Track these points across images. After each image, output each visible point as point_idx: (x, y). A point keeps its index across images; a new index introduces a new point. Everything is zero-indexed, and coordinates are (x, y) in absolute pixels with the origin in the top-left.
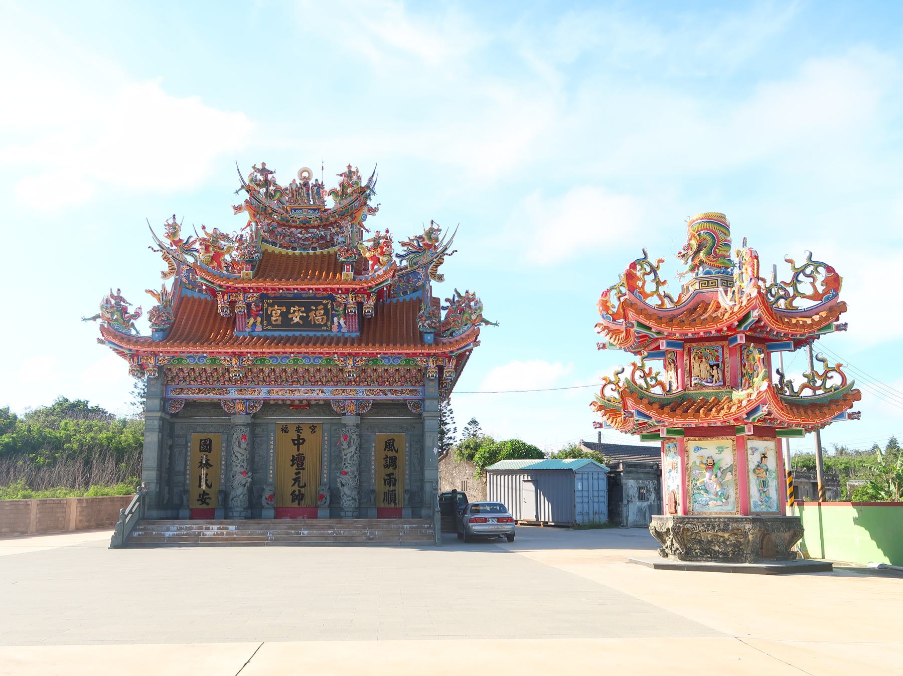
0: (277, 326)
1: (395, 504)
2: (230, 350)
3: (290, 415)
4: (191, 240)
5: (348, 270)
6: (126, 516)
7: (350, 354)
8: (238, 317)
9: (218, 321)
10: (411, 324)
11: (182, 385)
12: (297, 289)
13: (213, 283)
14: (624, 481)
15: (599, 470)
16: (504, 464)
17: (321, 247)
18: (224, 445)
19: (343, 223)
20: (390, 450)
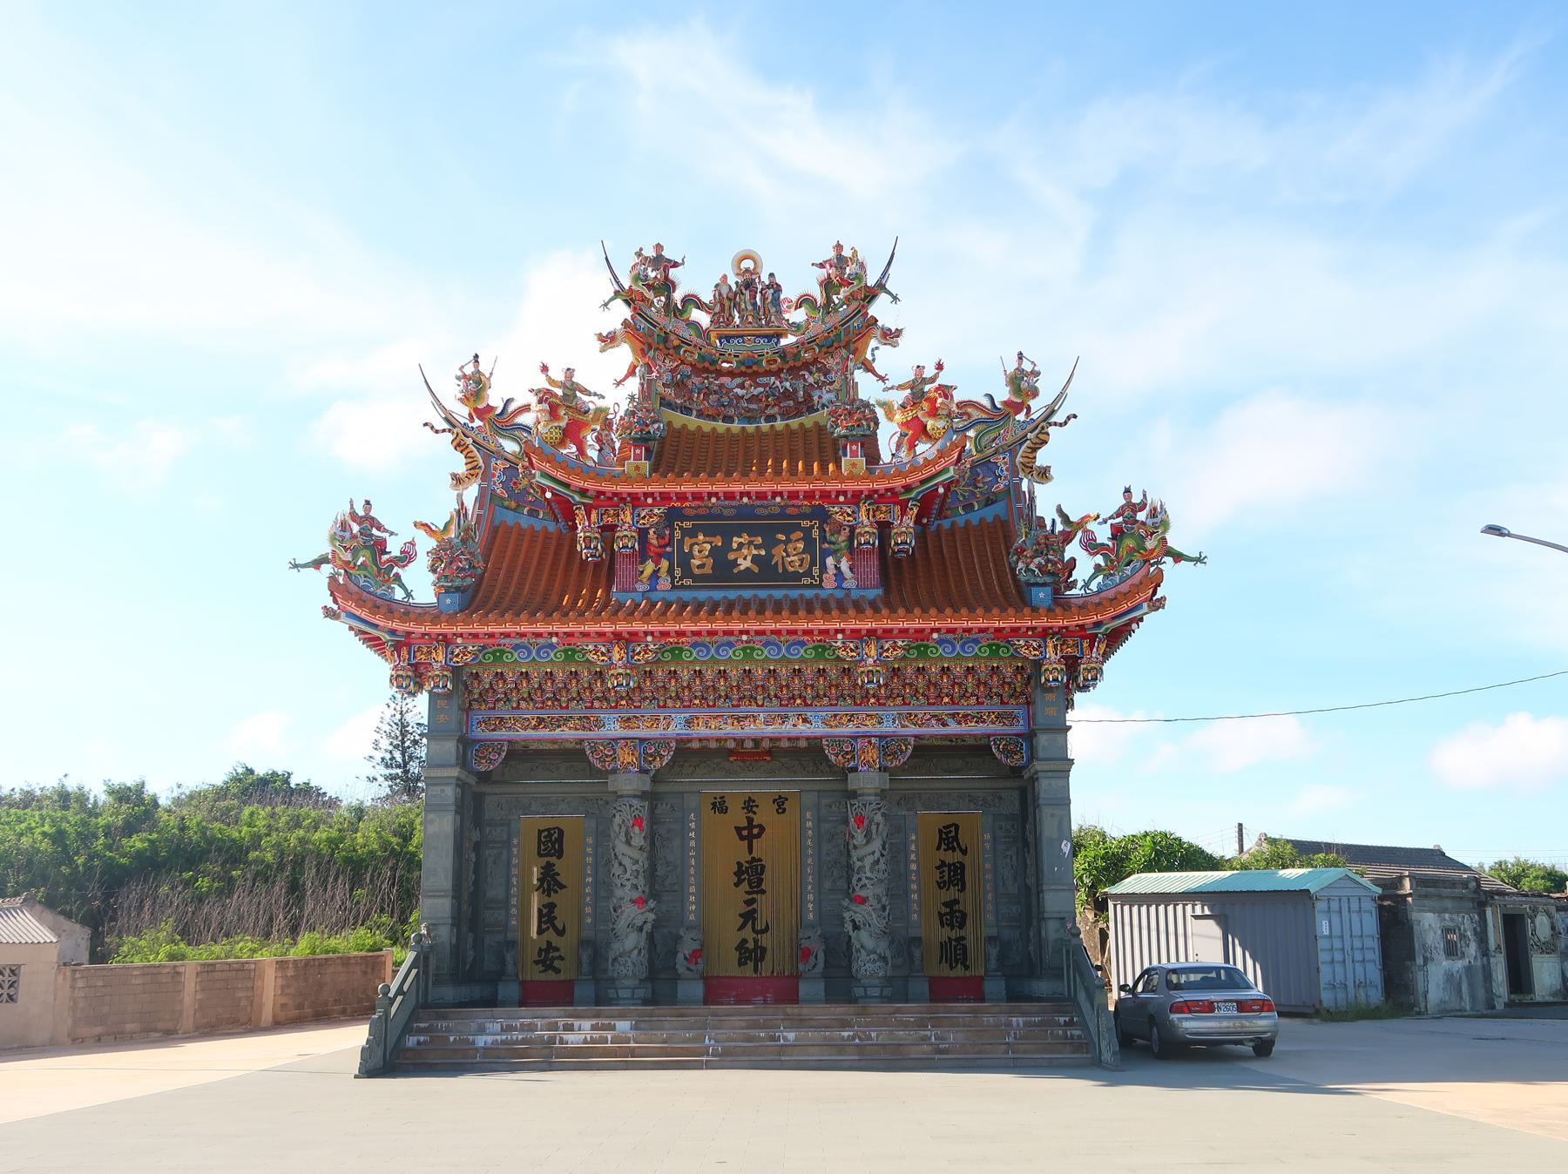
0: (703, 578)
1: (967, 967)
2: (607, 628)
3: (729, 773)
4: (512, 407)
5: (854, 454)
6: (392, 1001)
7: (871, 632)
8: (619, 560)
9: (574, 573)
10: (992, 577)
11: (503, 710)
12: (748, 494)
13: (567, 486)
14: (1415, 916)
15: (1362, 892)
16: (1138, 883)
17: (786, 415)
18: (590, 840)
19: (831, 362)
20: (950, 848)
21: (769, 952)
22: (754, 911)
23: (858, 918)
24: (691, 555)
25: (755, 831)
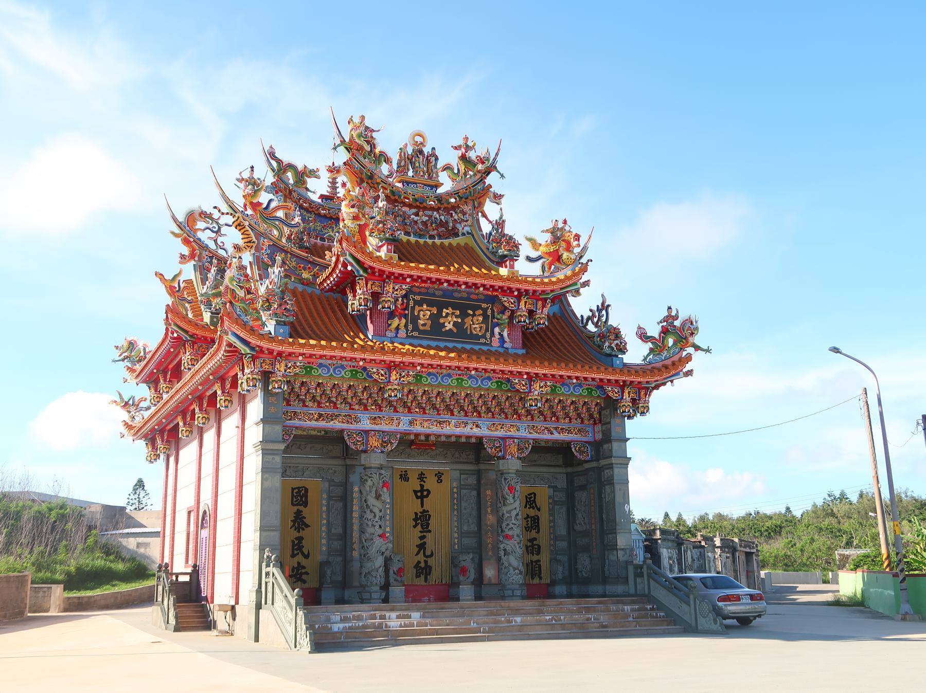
1: (540, 578)
3: (409, 456)
21: (433, 569)
22: (425, 543)
23: (508, 548)
24: (418, 318)
25: (425, 493)
